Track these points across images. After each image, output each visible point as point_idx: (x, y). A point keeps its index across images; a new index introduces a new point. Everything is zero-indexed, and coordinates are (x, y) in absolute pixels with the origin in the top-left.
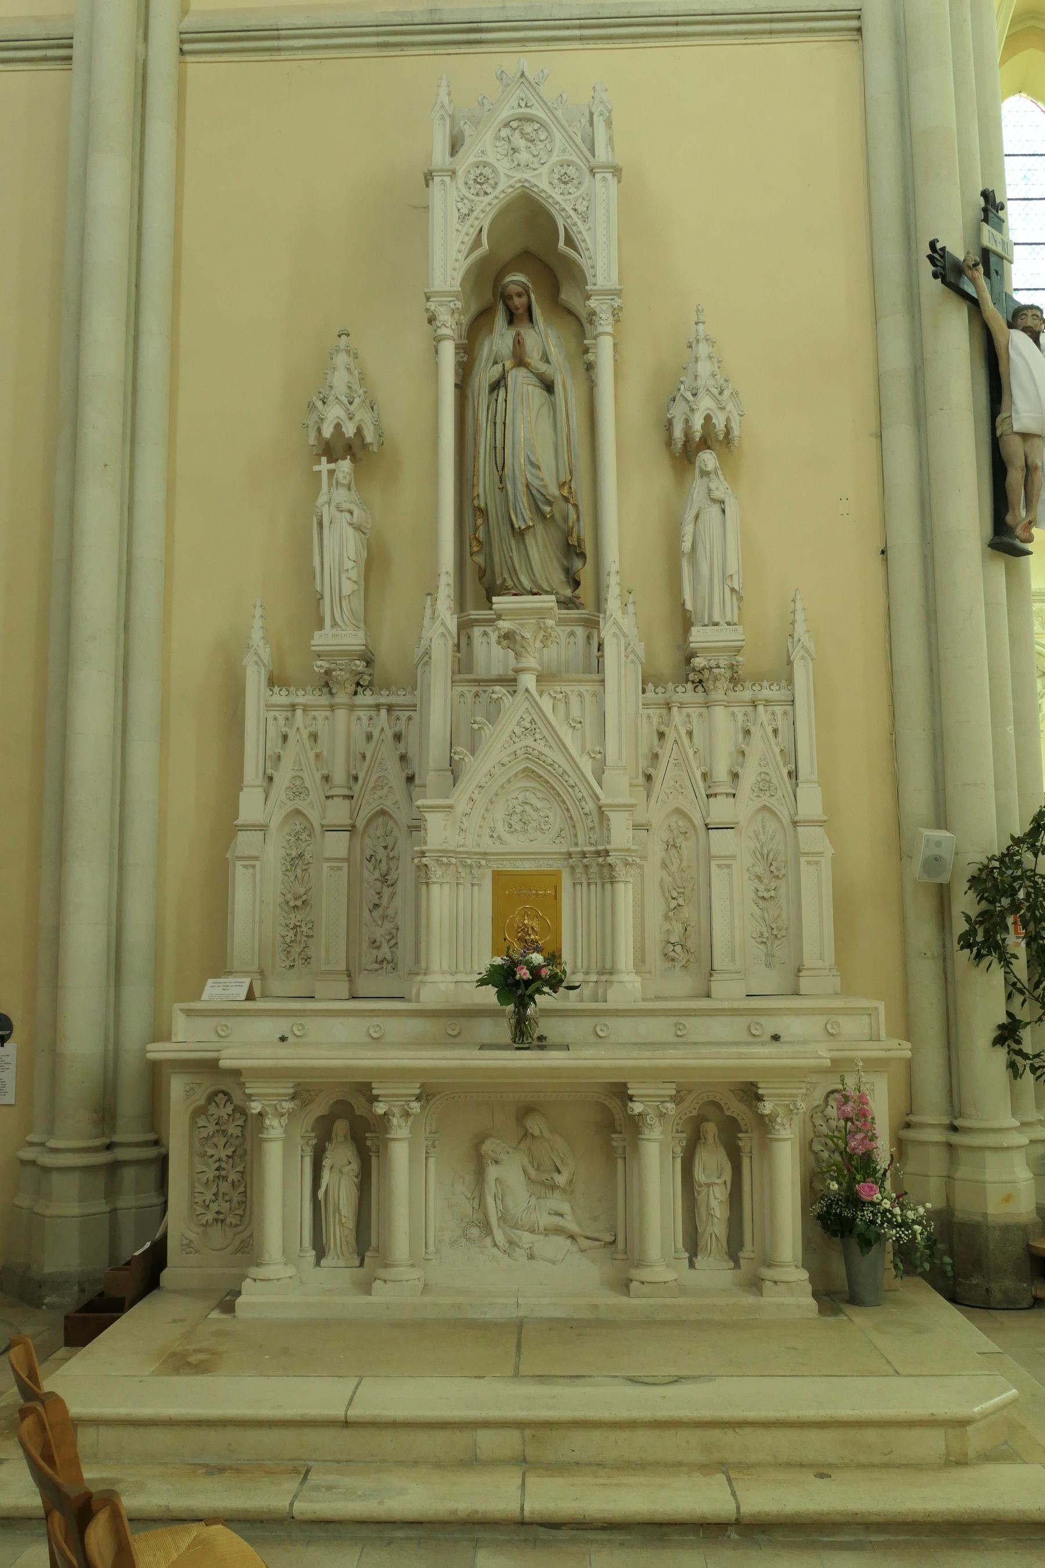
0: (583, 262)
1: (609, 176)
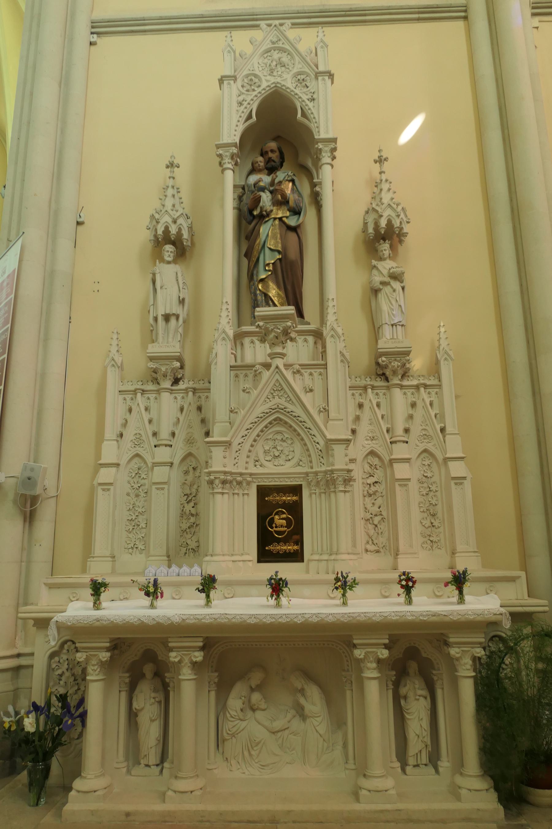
0: (312, 126)
1: (327, 78)
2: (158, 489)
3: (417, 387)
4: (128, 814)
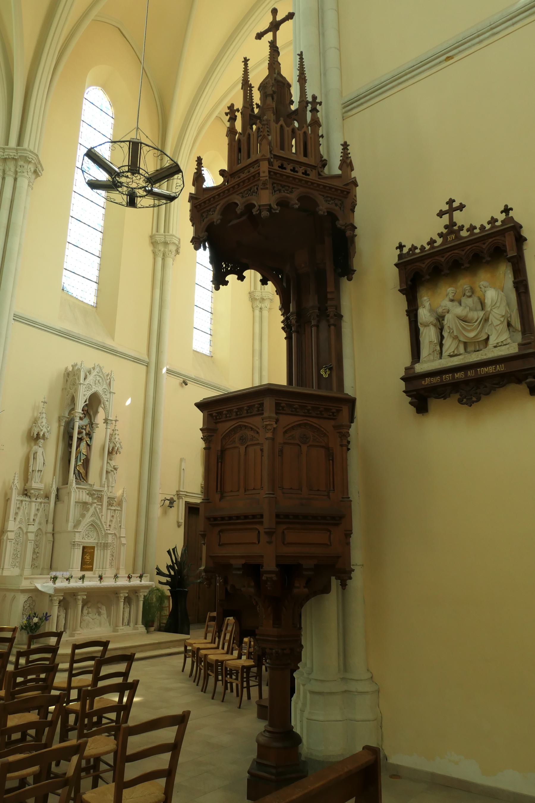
2: (30, 542)
3: (115, 510)
4: (67, 641)
